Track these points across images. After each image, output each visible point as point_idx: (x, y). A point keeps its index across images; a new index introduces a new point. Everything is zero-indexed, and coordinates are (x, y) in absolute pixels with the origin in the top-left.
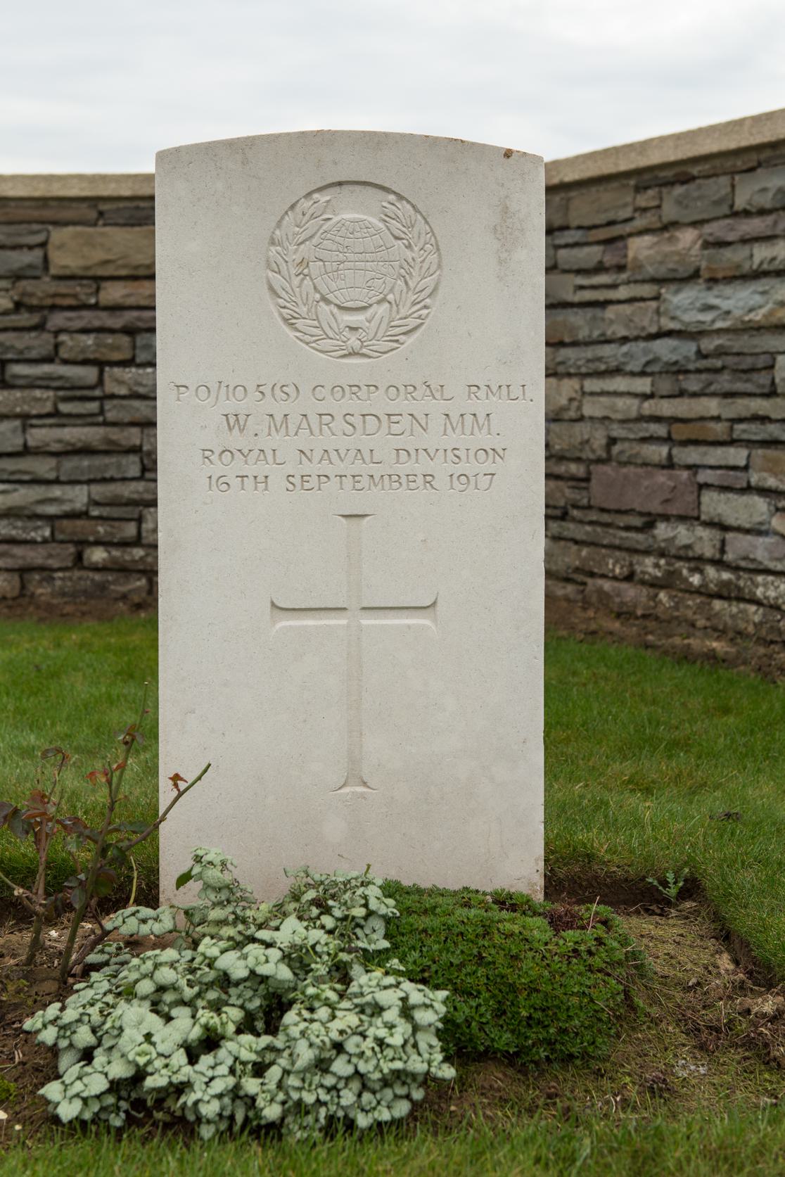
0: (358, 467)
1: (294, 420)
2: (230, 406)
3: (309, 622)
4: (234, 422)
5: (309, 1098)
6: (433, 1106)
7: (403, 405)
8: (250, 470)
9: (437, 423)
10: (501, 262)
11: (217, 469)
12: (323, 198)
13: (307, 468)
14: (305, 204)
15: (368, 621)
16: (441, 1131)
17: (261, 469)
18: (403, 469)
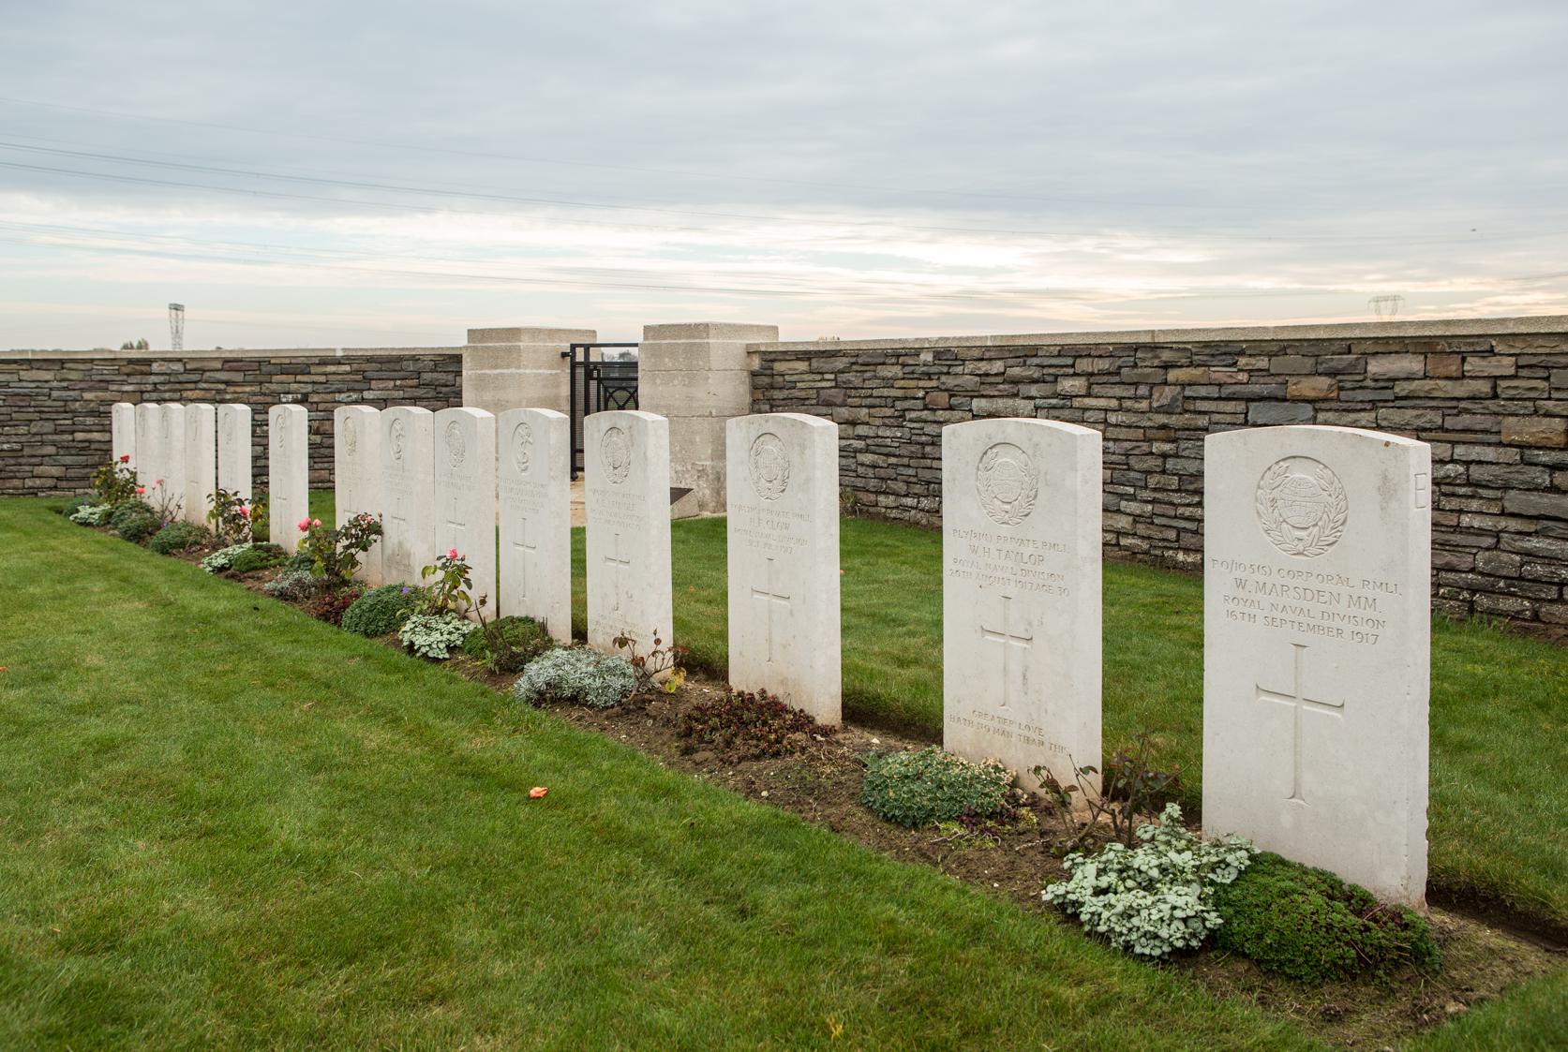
0: (1301, 618)
1: (1269, 586)
2: (1238, 573)
3: (1276, 700)
4: (1240, 584)
5: (1118, 929)
6: (1181, 957)
7: (1327, 587)
8: (1247, 610)
9: (1344, 600)
11: (1231, 606)
14: (1275, 468)
15: (1306, 707)
16: (682, 744)
17: (1254, 611)
18: (1326, 623)
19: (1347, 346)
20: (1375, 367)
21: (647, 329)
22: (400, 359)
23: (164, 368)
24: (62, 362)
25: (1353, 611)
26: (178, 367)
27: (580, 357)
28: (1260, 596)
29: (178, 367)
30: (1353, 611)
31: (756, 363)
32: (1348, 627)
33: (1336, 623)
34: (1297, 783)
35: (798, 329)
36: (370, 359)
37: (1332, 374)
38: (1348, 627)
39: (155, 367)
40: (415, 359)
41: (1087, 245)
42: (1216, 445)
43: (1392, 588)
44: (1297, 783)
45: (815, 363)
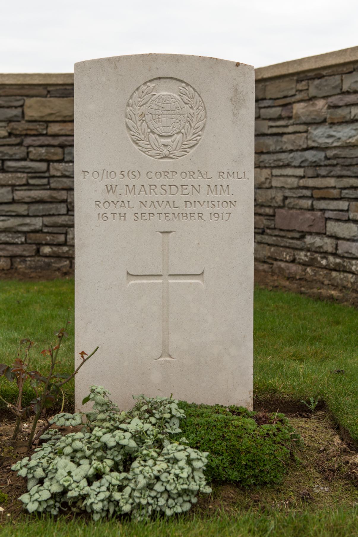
0: (168, 210)
2: (108, 181)
3: (145, 281)
4: (110, 188)
7: (189, 181)
8: (116, 211)
10: (234, 115)
12: (152, 85)
13: (144, 210)
14: (144, 88)
15: (172, 281)
25: (212, 197)
28: (130, 197)
30: (212, 197)
32: (206, 210)
33: (198, 209)
34: (165, 345)
38: (206, 210)
43: (241, 175)
44: (165, 345)
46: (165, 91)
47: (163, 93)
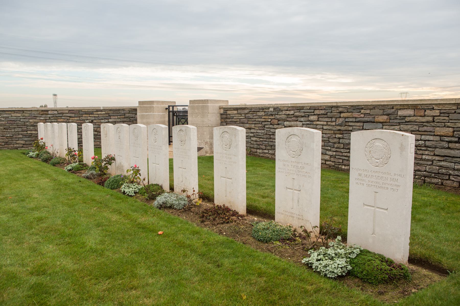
1: (368, 176)
3: (369, 208)
4: (360, 175)
5: (323, 270)
8: (362, 182)
10: (401, 153)
12: (373, 141)
13: (369, 183)
14: (371, 142)
15: (377, 209)
18: (383, 186)
19: (392, 107)
20: (400, 113)
21: (190, 101)
22: (119, 110)
23: (52, 112)
24: (23, 111)
26: (56, 112)
27: (171, 109)
29: (56, 112)
31: (222, 111)
35: (234, 102)
36: (110, 110)
37: (388, 115)
39: (49, 112)
40: (123, 110)
41: (318, 77)
42: (354, 135)
43: (402, 176)
45: (239, 111)
46: (378, 143)
47: (377, 144)
